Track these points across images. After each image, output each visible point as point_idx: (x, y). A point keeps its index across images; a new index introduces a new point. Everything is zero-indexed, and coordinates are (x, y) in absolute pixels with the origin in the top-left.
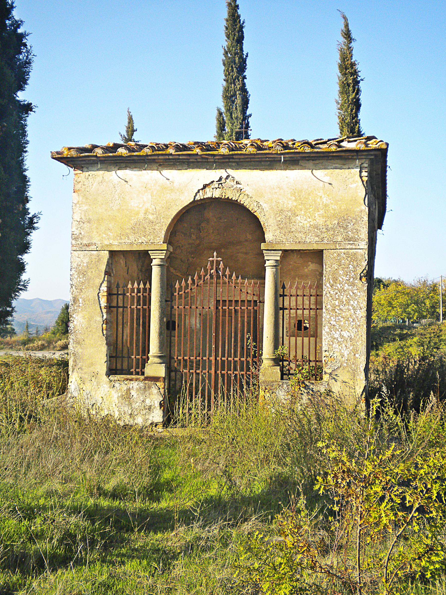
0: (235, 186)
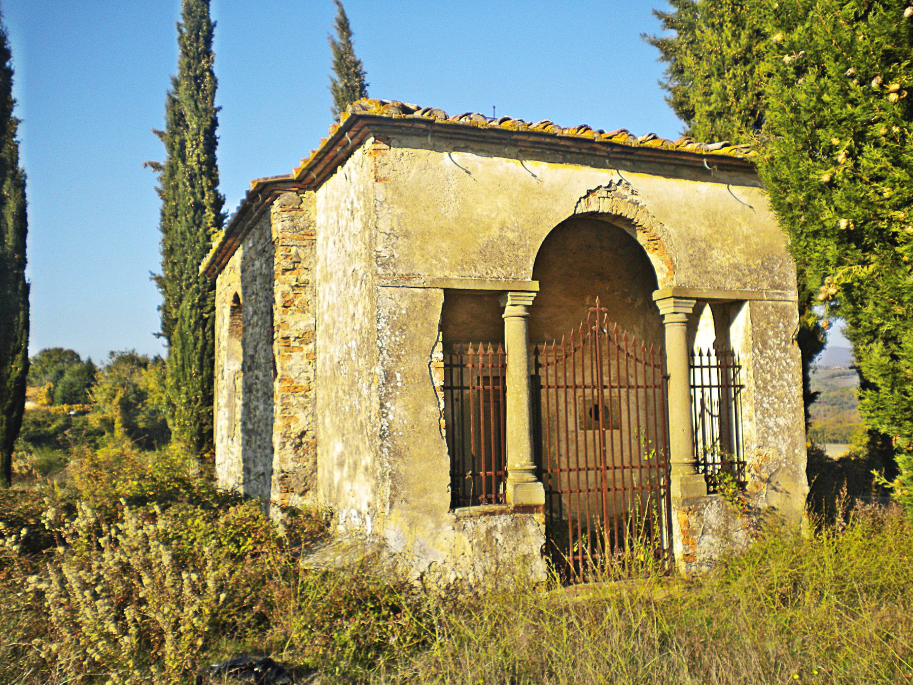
0: (629, 198)
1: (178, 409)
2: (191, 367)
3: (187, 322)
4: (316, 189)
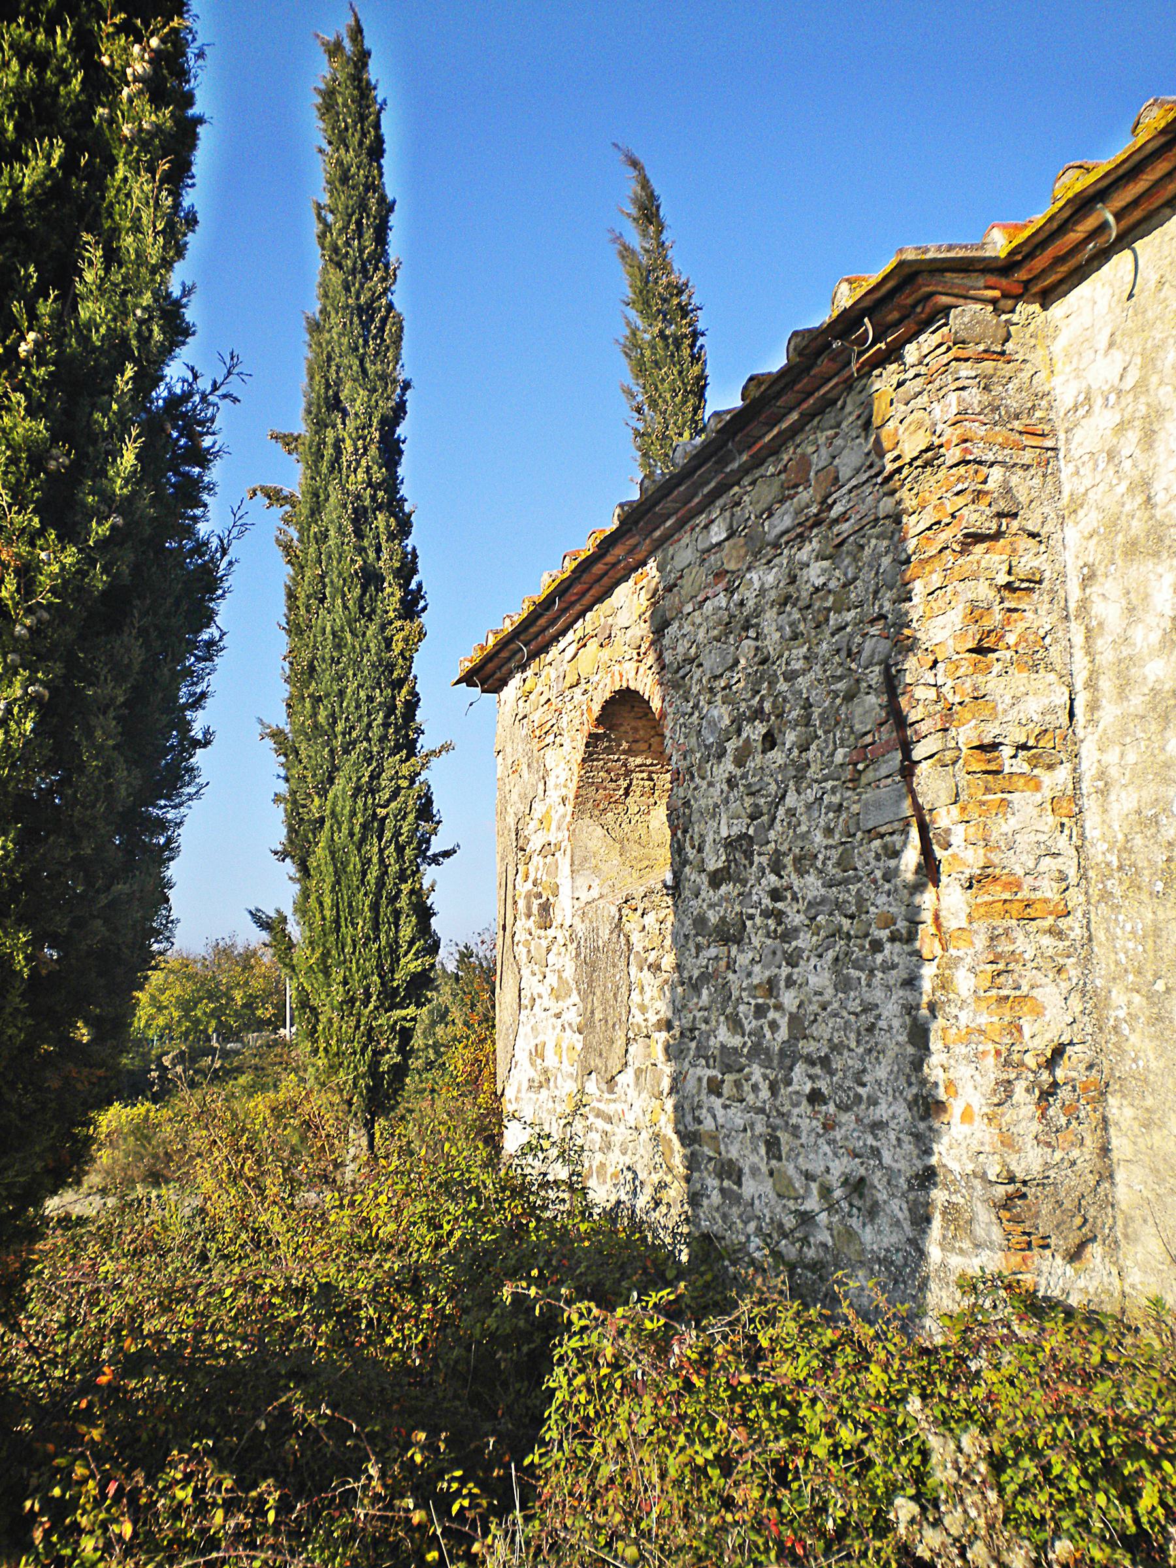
1: (323, 1019)
2: (354, 925)
3: (345, 826)
4: (1046, 298)
